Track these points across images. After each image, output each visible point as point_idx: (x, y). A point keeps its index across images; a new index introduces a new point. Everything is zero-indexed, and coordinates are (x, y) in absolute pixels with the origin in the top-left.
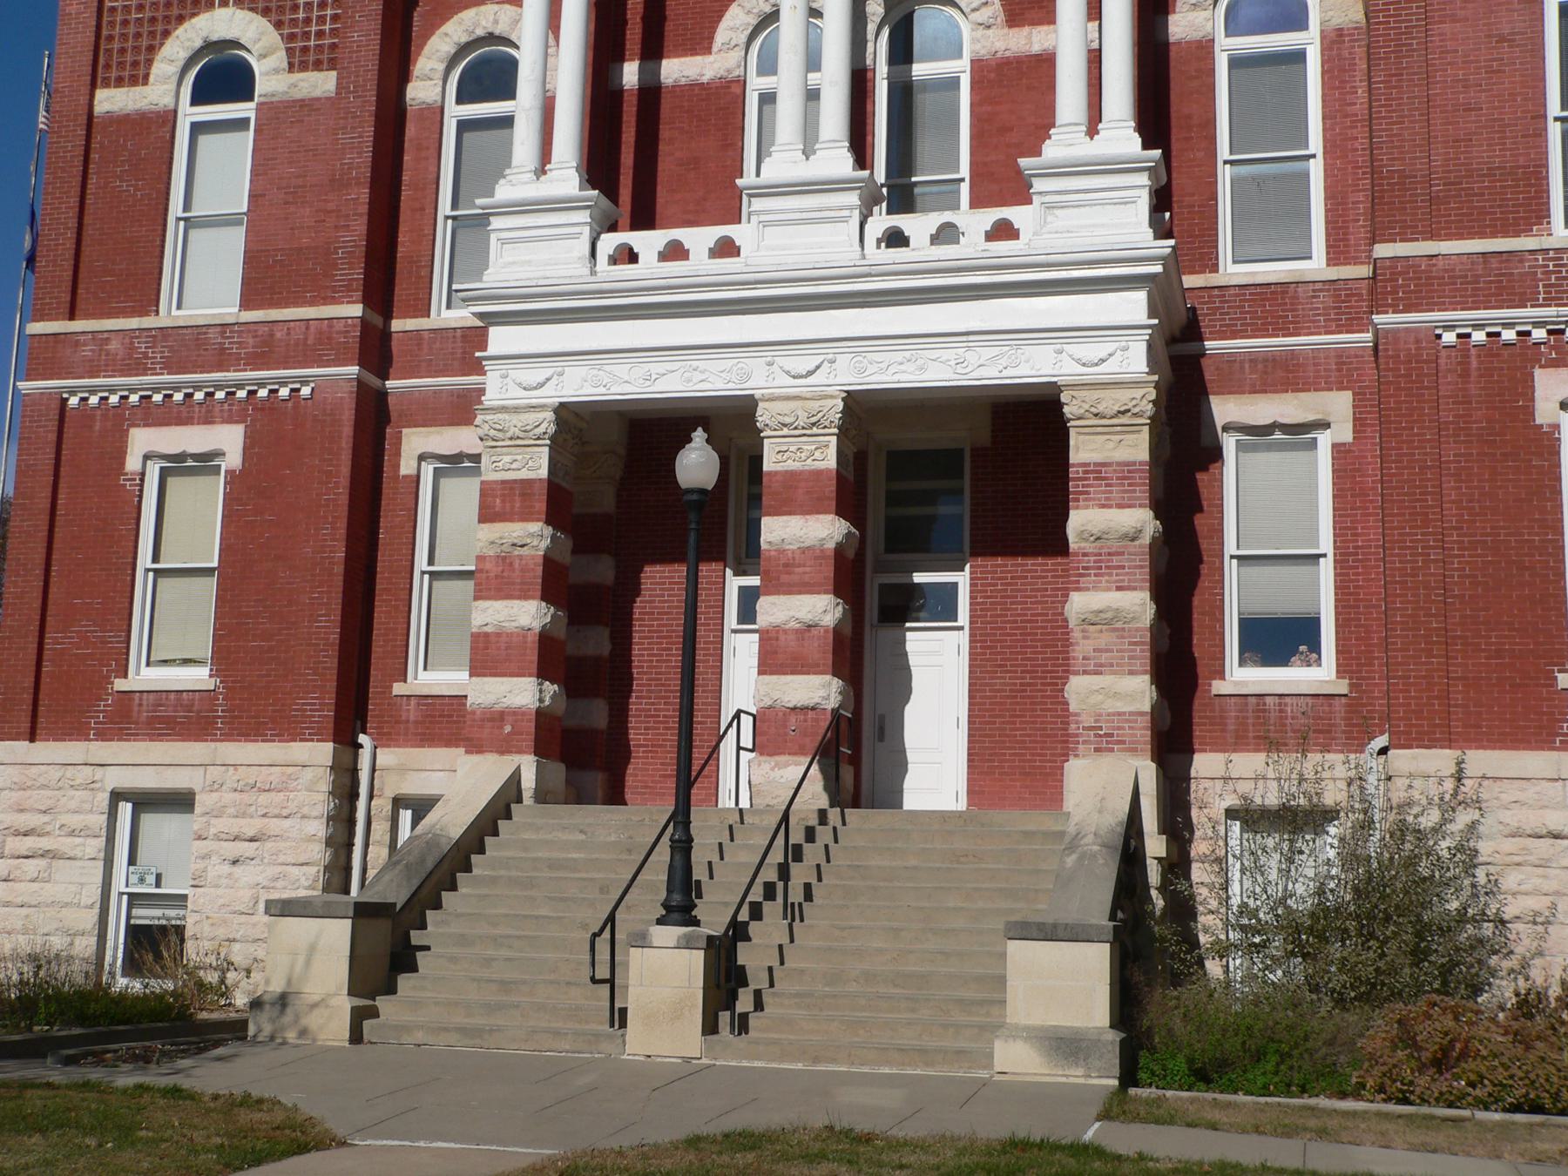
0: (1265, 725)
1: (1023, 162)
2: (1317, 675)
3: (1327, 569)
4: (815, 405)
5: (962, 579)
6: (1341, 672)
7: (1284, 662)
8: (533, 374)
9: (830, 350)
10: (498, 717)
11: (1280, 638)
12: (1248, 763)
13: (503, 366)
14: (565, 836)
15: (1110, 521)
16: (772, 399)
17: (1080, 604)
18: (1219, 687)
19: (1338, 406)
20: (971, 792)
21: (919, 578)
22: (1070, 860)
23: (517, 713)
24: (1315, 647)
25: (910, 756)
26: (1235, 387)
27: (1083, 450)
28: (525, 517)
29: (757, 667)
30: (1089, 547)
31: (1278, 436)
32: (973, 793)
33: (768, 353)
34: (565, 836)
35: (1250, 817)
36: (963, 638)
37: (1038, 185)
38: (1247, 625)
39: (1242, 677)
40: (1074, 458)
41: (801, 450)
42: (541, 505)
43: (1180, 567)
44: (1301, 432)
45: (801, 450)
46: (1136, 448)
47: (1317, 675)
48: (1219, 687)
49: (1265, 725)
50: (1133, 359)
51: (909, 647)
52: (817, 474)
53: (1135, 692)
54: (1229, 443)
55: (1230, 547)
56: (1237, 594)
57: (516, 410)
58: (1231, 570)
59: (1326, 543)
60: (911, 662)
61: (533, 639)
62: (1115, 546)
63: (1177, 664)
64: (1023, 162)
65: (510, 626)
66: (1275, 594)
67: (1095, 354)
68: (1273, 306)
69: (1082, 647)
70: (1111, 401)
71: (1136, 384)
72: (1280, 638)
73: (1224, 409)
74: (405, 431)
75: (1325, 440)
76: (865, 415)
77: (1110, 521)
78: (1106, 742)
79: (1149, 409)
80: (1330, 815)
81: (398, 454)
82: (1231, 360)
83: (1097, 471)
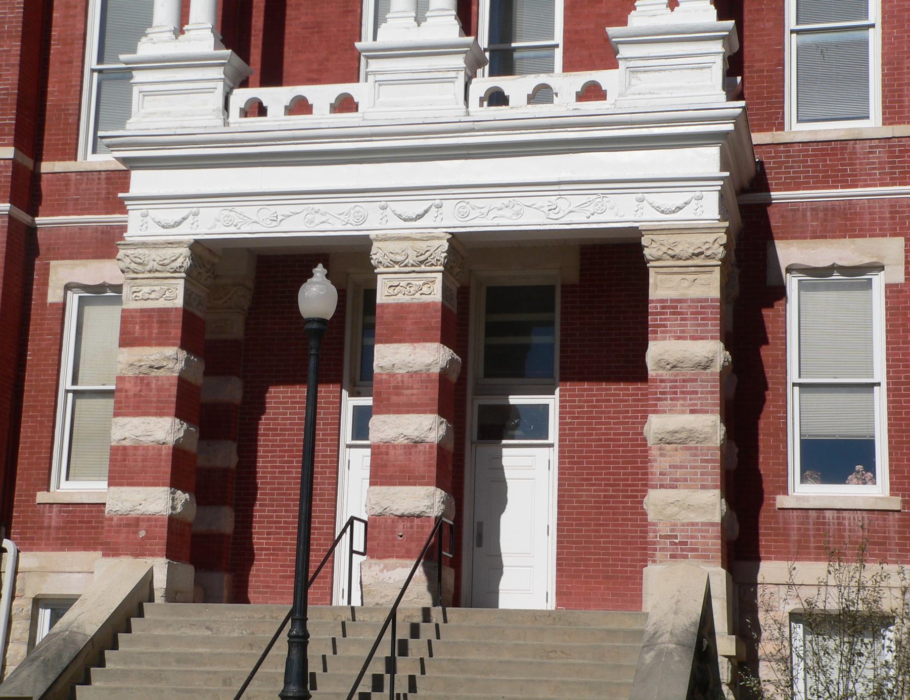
0: (825, 537)
1: (611, 31)
2: (873, 492)
3: (880, 398)
4: (423, 245)
5: (553, 401)
6: (895, 489)
7: (841, 479)
8: (171, 214)
9: (436, 196)
10: (133, 523)
11: (838, 458)
12: (811, 571)
13: (144, 206)
14: (190, 632)
15: (682, 350)
16: (385, 239)
17: (657, 425)
18: (782, 501)
19: (891, 250)
20: (559, 593)
21: (514, 400)
22: (649, 657)
23: (150, 520)
24: (870, 467)
25: (506, 560)
26: (798, 233)
27: (661, 288)
28: (162, 342)
29: (368, 477)
30: (666, 374)
31: (836, 277)
32: (561, 593)
33: (383, 199)
34: (190, 632)
35: (812, 620)
36: (552, 455)
37: (624, 51)
38: (808, 446)
39: (803, 492)
40: (653, 294)
41: (410, 285)
42: (176, 331)
43: (747, 394)
44: (857, 274)
45: (410, 285)
46: (709, 286)
47: (873, 492)
48: (782, 501)
49: (825, 537)
50: (707, 207)
51: (505, 462)
52: (425, 306)
53: (707, 505)
54: (792, 283)
55: (793, 376)
56: (800, 418)
57: (155, 245)
58: (794, 396)
59: (880, 373)
60: (508, 474)
61: (166, 452)
62: (689, 373)
63: (744, 481)
64: (611, 31)
65: (147, 440)
66: (833, 419)
67: (674, 202)
68: (833, 161)
69: (659, 464)
70: (686, 245)
71: (709, 230)
72: (838, 458)
73: (788, 253)
74: (53, 263)
75: (879, 281)
76: (468, 254)
77: (682, 350)
78: (681, 549)
79: (720, 252)
80: (887, 620)
81: (46, 284)
82: (794, 209)
83: (673, 306)
